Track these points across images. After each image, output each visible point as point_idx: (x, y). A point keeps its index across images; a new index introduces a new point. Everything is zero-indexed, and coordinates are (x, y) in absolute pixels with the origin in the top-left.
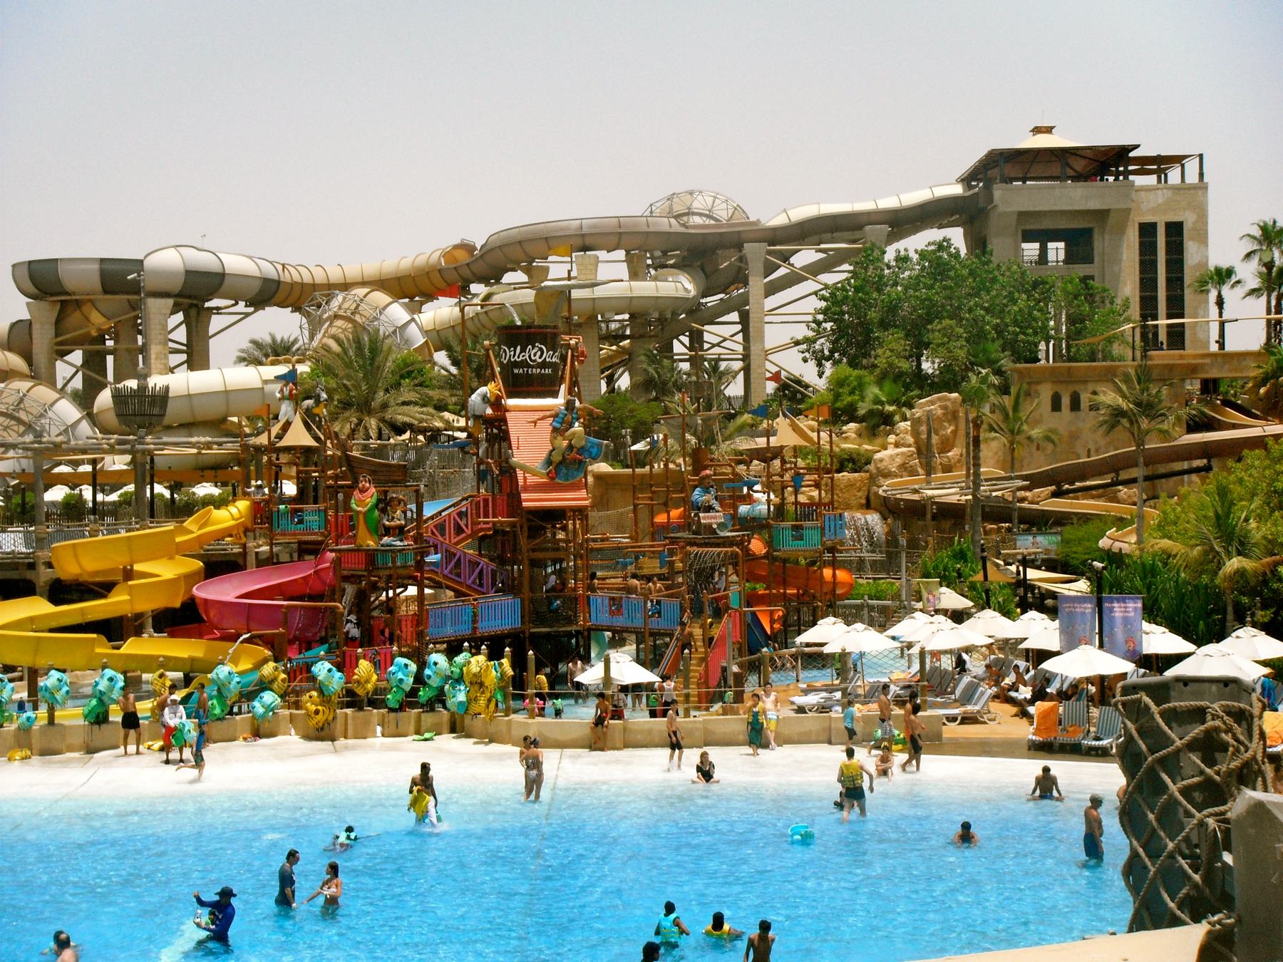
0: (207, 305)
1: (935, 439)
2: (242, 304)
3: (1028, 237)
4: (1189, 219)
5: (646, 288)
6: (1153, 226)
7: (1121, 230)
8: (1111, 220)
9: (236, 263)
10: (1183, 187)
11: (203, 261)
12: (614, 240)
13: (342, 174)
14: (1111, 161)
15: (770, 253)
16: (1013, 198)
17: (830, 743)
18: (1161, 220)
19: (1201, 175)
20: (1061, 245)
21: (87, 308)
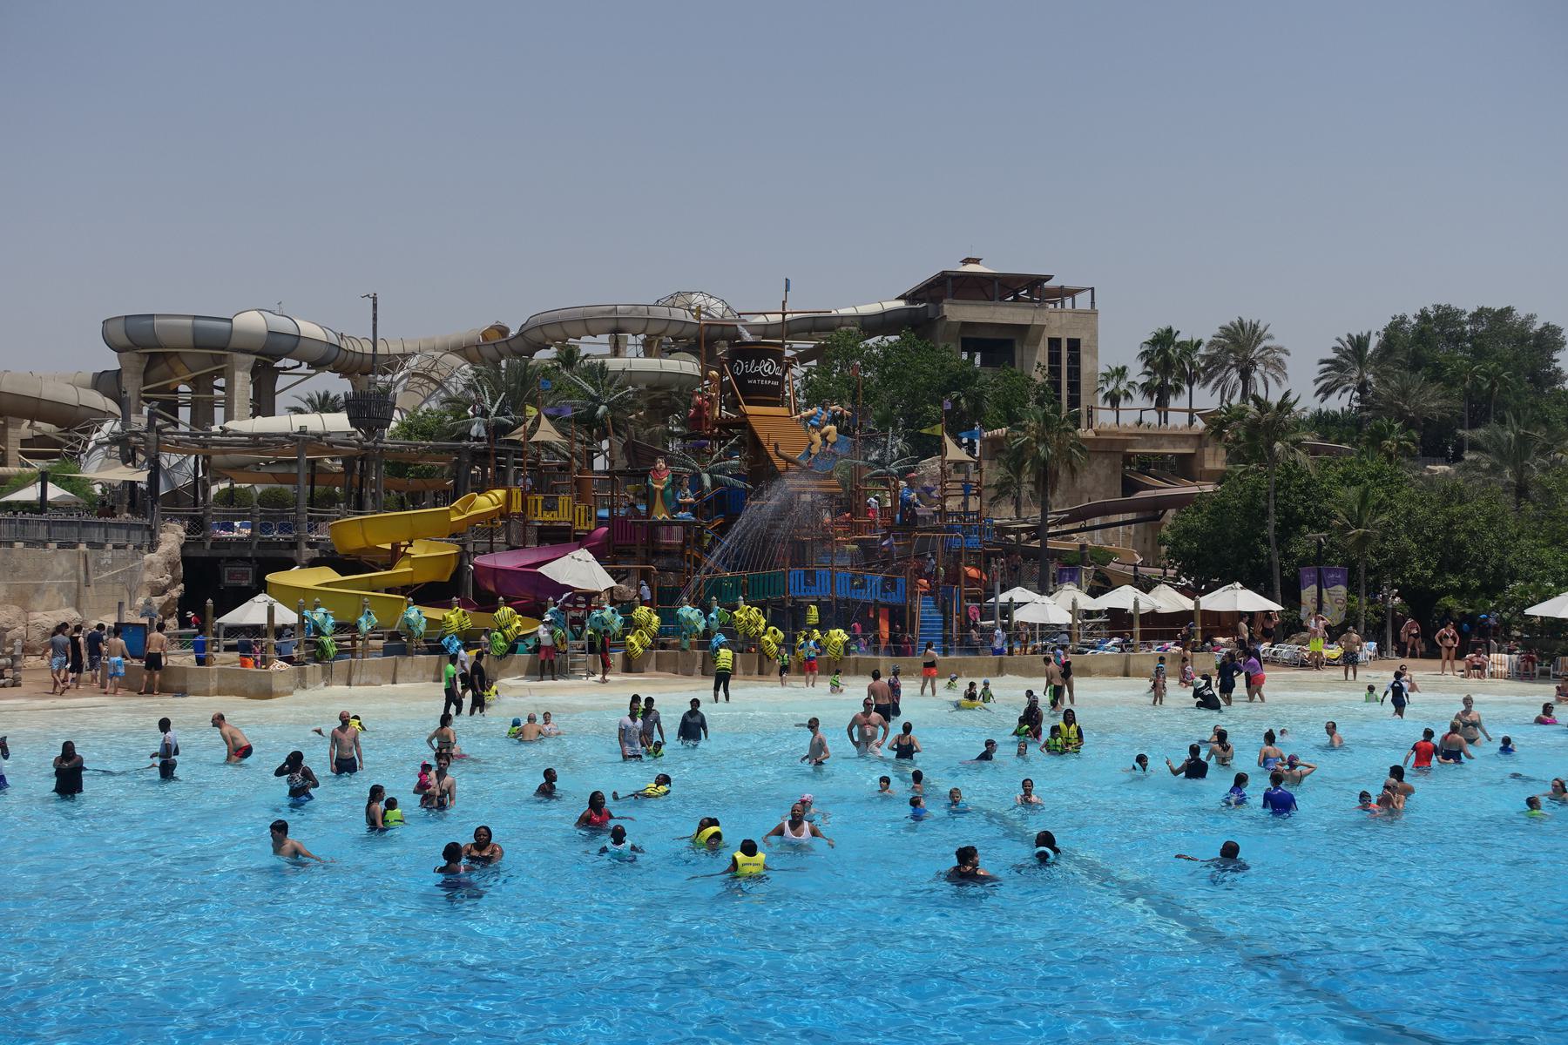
0: (278, 365)
6: (1059, 340)
7: (1036, 343)
8: (1032, 334)
9: (309, 329)
11: (283, 325)
12: (642, 325)
13: (409, 250)
14: (1032, 288)
16: (959, 312)
17: (1126, 674)
19: (1093, 303)
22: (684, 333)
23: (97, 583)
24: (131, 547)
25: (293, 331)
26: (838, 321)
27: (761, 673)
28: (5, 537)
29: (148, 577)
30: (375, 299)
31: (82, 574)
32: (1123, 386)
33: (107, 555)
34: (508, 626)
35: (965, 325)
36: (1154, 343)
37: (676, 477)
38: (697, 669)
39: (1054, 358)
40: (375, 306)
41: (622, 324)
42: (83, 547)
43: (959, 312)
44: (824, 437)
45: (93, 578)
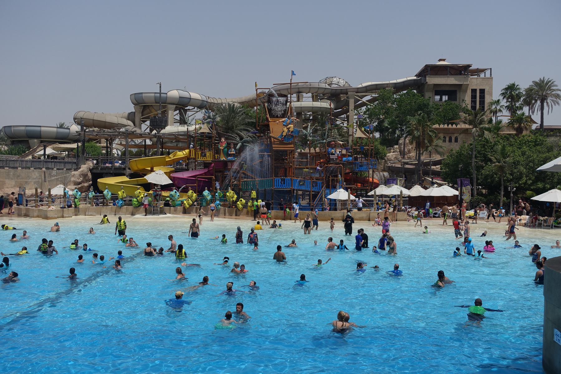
1: (406, 150)
2: (196, 108)
3: (437, 93)
4: (487, 89)
5: (318, 104)
6: (476, 90)
7: (466, 91)
9: (194, 95)
10: (485, 78)
11: (185, 94)
12: (308, 90)
15: (356, 96)
16: (432, 80)
17: (369, 220)
18: (478, 88)
19: (491, 74)
20: (447, 97)
21: (151, 108)
22: (325, 92)
23: (49, 181)
24: (65, 169)
25: (188, 96)
26: (386, 86)
27: (236, 215)
28: (2, 165)
29: (73, 179)
30: (160, 84)
31: (43, 178)
32: (498, 108)
33: (54, 172)
34: (139, 196)
35: (435, 85)
36: (506, 89)
37: (229, 144)
38: (234, 214)
39: (474, 97)
40: (160, 87)
41: (300, 90)
42: (44, 169)
43: (432, 80)
44: (288, 129)
45: (47, 179)
